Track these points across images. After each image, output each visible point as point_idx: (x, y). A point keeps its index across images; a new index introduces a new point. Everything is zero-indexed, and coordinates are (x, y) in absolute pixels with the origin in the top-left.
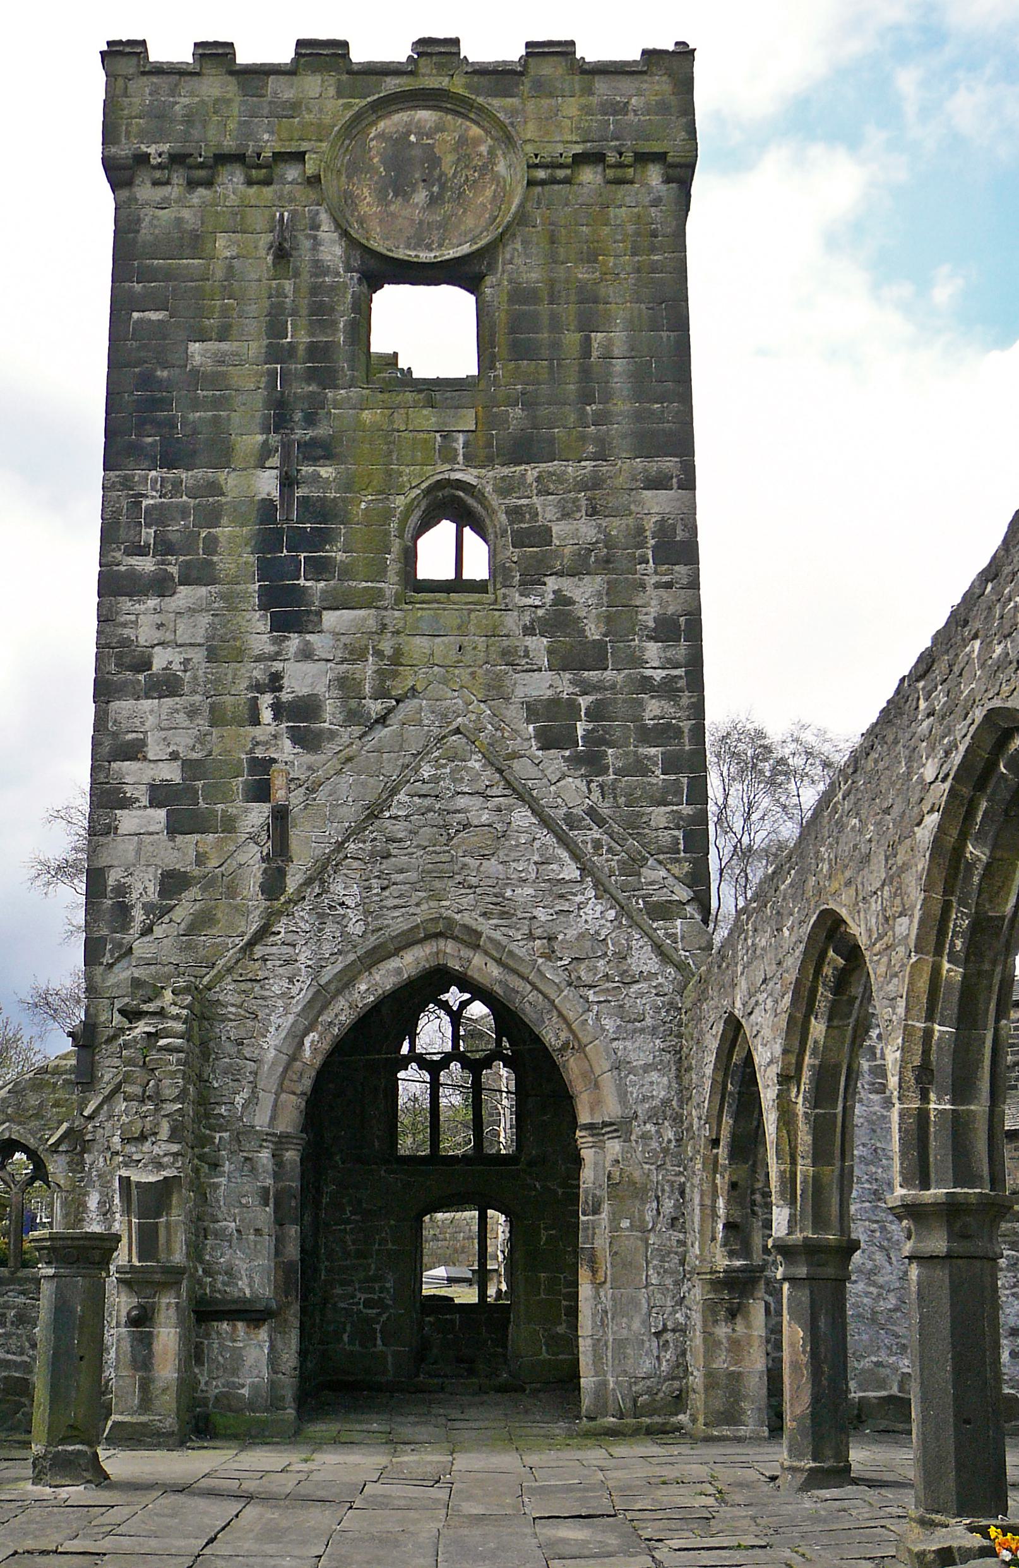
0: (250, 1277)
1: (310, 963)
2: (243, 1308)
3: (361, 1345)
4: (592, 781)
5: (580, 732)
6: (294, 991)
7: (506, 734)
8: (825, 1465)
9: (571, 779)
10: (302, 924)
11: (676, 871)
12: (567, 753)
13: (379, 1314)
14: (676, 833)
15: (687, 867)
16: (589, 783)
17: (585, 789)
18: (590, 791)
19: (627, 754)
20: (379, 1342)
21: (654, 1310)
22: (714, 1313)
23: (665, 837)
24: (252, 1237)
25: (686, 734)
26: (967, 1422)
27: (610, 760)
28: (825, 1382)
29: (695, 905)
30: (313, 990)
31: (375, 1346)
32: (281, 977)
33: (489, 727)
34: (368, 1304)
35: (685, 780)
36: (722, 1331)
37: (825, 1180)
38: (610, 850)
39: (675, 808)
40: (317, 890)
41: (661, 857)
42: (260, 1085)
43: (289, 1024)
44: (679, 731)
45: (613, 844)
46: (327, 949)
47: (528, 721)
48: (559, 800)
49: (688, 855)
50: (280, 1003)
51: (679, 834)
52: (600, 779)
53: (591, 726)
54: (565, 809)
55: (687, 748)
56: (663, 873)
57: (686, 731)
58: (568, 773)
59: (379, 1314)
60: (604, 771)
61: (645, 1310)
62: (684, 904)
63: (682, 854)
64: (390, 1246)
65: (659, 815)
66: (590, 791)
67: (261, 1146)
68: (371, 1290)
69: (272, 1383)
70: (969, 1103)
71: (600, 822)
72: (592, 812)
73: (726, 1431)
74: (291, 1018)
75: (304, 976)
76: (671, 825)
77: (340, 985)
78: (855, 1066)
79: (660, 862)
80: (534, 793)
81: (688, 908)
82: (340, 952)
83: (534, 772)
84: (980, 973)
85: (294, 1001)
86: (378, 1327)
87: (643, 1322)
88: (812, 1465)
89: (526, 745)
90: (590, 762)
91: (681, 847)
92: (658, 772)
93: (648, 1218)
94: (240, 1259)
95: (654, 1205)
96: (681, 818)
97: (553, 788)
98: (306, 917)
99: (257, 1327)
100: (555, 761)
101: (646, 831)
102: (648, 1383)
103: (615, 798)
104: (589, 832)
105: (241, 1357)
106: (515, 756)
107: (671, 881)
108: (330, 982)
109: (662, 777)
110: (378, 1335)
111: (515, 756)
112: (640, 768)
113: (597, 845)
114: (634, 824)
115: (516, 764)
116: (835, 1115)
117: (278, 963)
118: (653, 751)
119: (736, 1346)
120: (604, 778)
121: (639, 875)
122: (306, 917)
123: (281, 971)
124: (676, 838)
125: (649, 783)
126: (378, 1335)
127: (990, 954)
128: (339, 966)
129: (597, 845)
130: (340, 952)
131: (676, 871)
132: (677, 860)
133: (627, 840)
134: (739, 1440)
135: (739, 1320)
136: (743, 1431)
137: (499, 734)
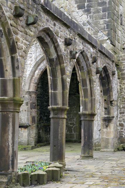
0: (24, 119)
1: (34, 57)
2: (23, 125)
3: (70, 133)
4: (88, 15)
5: (86, 5)
6: (32, 63)
7: (71, 7)
8: (85, 155)
9: (84, 15)
10: (33, 50)
11: (105, 33)
12: (83, 10)
13: (73, 126)
14: (105, 25)
15: (107, 32)
16: (87, 16)
17: (87, 17)
18: (88, 17)
19: (95, 9)
20: (73, 132)
21: (99, 126)
22: (103, 126)
23: (102, 26)
24: (24, 112)
25: (107, 3)
26: (55, 146)
27: (92, 10)
28: (86, 140)
29: (109, 40)
30: (35, 63)
31: (72, 132)
32: (29, 60)
33: (68, 6)
34: (71, 124)
35: (107, 13)
36: (105, 130)
37: (87, 101)
38: (91, 30)
39: (105, 19)
40: (36, 43)
41: (102, 30)
42: (26, 82)
43: (31, 70)
44: (106, 3)
45: (92, 29)
46: (38, 54)
47: (76, 4)
48: (82, 20)
49: (107, 29)
50: (29, 66)
51: (105, 25)
52: (90, 15)
53: (88, 3)
54: (83, 22)
55: (107, 6)
56: (102, 34)
57: (107, 2)
58: (83, 14)
59: (73, 126)
60: (90, 13)
61: (97, 126)
62: (107, 40)
63: (106, 29)
64: (75, 112)
65: (102, 21)
66: (88, 17)
67: (26, 94)
68: (72, 121)
69: (28, 140)
70: (56, 91)
71: (90, 24)
72: (88, 22)
73: (105, 150)
74: (31, 68)
75: (34, 60)
76: (104, 23)
77: (41, 61)
78: (92, 79)
79: (102, 31)
80: (77, 19)
81: (107, 41)
82: (40, 55)
83: (77, 14)
84: (53, 68)
85: (32, 65)
86: (73, 129)
87: (97, 128)
88: (84, 155)
89: (75, 9)
90: (88, 11)
91: (106, 28)
92: (101, 12)
93: (98, 107)
94: (22, 116)
95: (99, 104)
96: (106, 22)
97: (81, 17)
98: (34, 48)
99: (26, 129)
100: (81, 12)
101: (99, 25)
102: (98, 140)
103: (93, 18)
104: (87, 26)
105: (23, 135)
106: (73, 11)
107: (104, 35)
108: (39, 61)
109: (102, 13)
110: (73, 130)
111: (73, 11)
112: (98, 11)
113: (89, 29)
114: (96, 24)
115: (73, 13)
116: (87, 89)
117: (29, 58)
118: (100, 7)
119: (108, 133)
120: (91, 14)
121: (97, 35)
122: (34, 48)
123: (29, 59)
124: (105, 26)
125: (100, 15)
126: (73, 130)
127: (54, 65)
128: (40, 58)
129: (89, 29)
130: (40, 55)
131: (105, 33)
132: (105, 31)
133: (95, 27)
134: (107, 152)
135: (108, 127)
136: (108, 150)
137: (70, 7)
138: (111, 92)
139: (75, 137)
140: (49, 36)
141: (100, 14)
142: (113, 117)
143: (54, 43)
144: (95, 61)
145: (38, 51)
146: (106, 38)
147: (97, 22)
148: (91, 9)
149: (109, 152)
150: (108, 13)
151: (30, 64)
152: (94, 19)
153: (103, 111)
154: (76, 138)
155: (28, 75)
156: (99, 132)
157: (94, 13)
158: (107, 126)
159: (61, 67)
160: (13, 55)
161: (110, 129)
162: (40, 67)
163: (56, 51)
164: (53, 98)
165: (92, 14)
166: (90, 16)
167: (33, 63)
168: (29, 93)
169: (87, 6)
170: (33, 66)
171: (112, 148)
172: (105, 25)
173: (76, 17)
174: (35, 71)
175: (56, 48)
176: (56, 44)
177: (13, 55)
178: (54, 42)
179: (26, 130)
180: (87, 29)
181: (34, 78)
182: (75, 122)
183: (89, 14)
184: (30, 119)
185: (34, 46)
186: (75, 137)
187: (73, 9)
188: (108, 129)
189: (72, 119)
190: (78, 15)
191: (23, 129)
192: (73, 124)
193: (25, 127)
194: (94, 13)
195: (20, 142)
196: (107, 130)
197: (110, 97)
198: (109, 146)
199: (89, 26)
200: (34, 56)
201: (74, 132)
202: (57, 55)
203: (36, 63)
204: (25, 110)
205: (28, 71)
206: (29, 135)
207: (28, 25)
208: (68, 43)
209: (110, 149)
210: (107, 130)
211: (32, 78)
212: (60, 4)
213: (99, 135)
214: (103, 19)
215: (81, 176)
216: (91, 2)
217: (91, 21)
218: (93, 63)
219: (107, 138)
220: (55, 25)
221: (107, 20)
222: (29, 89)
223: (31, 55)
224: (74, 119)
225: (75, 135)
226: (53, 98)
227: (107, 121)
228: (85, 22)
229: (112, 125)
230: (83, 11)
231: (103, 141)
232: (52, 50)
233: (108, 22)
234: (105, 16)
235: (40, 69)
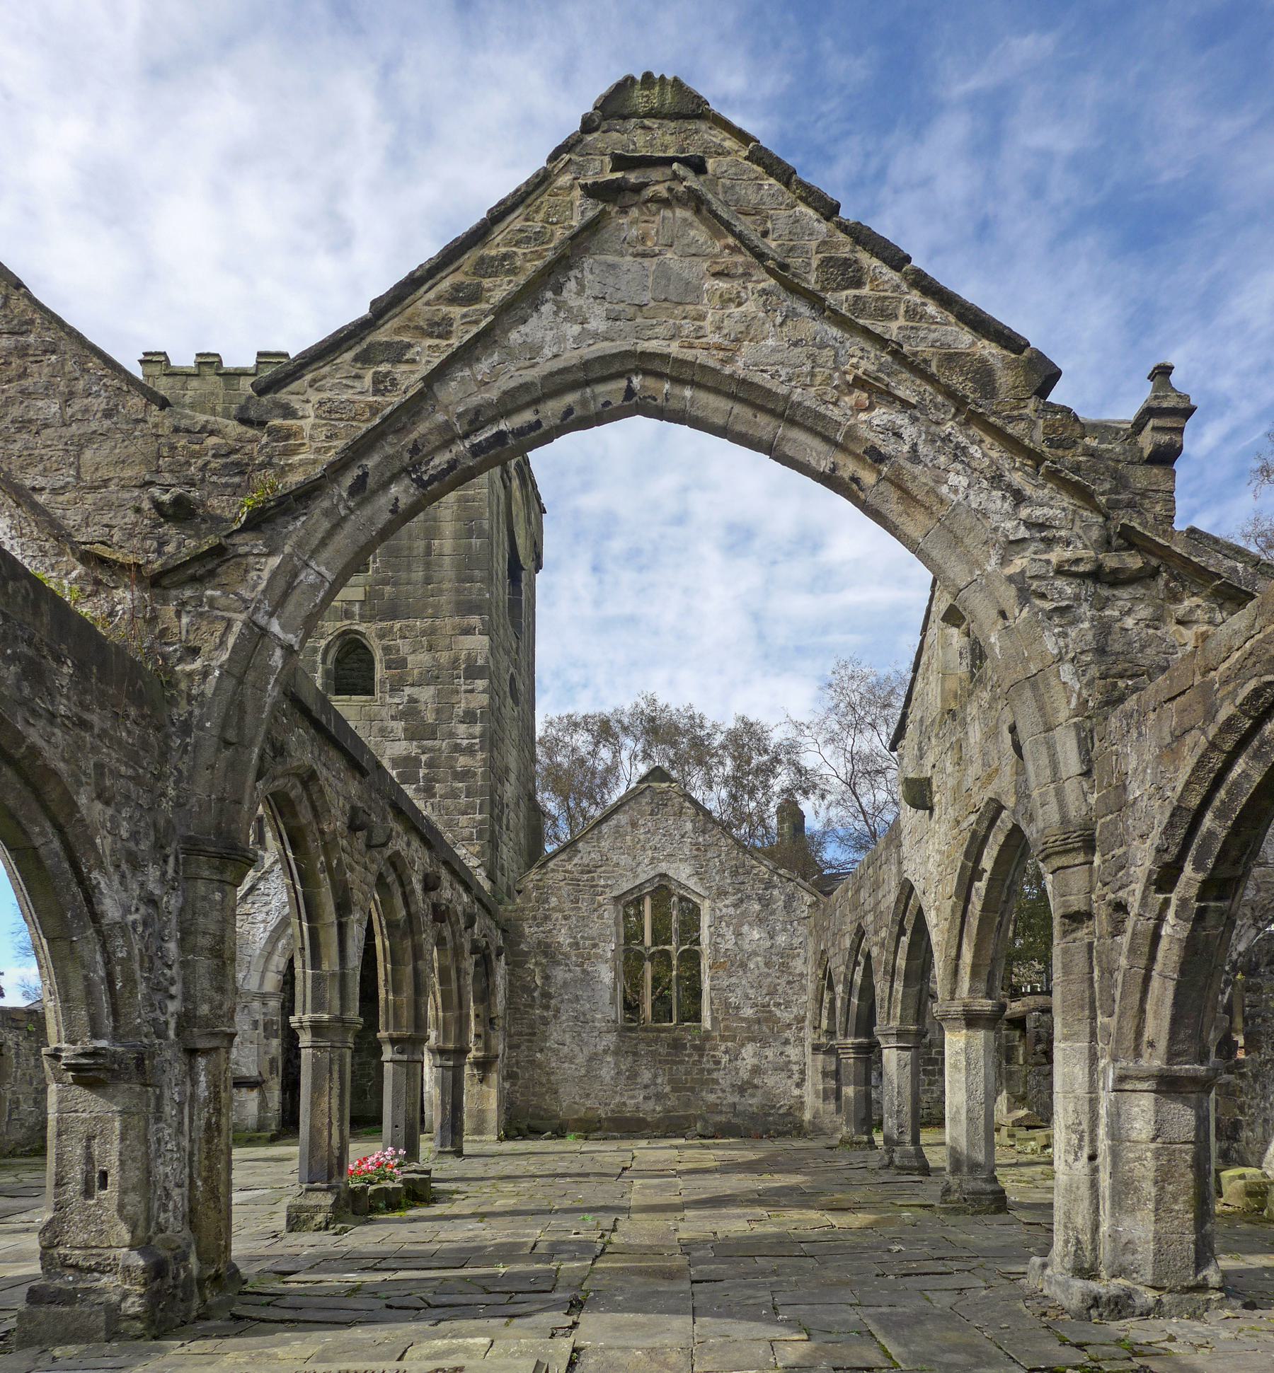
11: (471, 849)
23: (466, 832)
60: (434, 796)
65: (463, 820)
112: (454, 794)
118: (461, 785)
138: (992, 1046)
140: (395, 870)
142: (497, 1056)
143: (402, 885)
144: (470, 923)
147: (452, 820)
151: (263, 921)
155: (258, 951)
159: (413, 941)
160: (344, 920)
163: (407, 904)
164: (391, 1012)
175: (407, 898)
176: (408, 888)
177: (344, 920)
178: (403, 882)
184: (266, 1065)
191: (244, 1090)
197: (489, 1008)
202: (409, 913)
206: (263, 1105)
207: (369, 846)
208: (431, 884)
218: (466, 928)
220: (408, 844)
221: (478, 817)
222: (261, 985)
226: (391, 1012)
232: (398, 901)
233: (482, 822)
234: (474, 808)
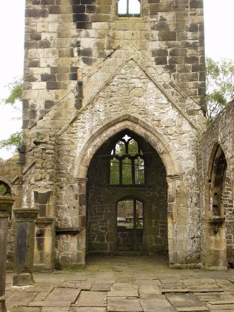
2: (69, 230)
5: (168, 59)
6: (85, 136)
10: (87, 116)
12: (164, 66)
13: (105, 232)
15: (199, 99)
16: (170, 75)
18: (170, 77)
22: (210, 232)
23: (193, 91)
27: (177, 68)
30: (90, 136)
34: (102, 229)
35: (199, 74)
36: (213, 238)
38: (176, 95)
40: (91, 107)
44: (197, 59)
46: (94, 124)
47: (153, 56)
50: (81, 140)
53: (171, 57)
56: (192, 101)
59: (105, 232)
60: (175, 71)
65: (191, 84)
66: (170, 77)
71: (173, 86)
72: (171, 83)
74: (84, 144)
75: (88, 132)
79: (191, 98)
81: (199, 111)
83: (154, 71)
89: (152, 63)
90: (171, 68)
92: (191, 71)
95: (190, 199)
97: (160, 76)
99: (74, 236)
100: (160, 68)
106: (148, 67)
107: (194, 104)
111: (148, 67)
112: (185, 70)
113: (173, 93)
114: (183, 87)
115: (149, 69)
118: (189, 65)
119: (217, 243)
120: (175, 73)
123: (80, 130)
131: (196, 101)
132: (196, 97)
135: (218, 234)
137: (144, 60)
139: (109, 248)
141: (189, 74)
145: (94, 120)
146: (198, 107)
147: (185, 84)
148: (175, 66)
149: (220, 271)
150: (201, 74)
151: (81, 138)
152: (180, 80)
153: (209, 210)
154: (110, 248)
156: (191, 241)
157: (180, 71)
158: (216, 233)
161: (220, 236)
162: (95, 143)
165: (177, 73)
166: (174, 76)
167: (87, 136)
168: (80, 181)
169: (169, 61)
170: (86, 141)
171: (224, 265)
172: (197, 90)
173: (153, 75)
174: (88, 148)
179: (75, 239)
180: (170, 93)
181: (85, 158)
182: (109, 227)
183: (173, 72)
185: (88, 111)
186: (109, 248)
187: (149, 63)
188: (217, 237)
189: (104, 221)
190: (156, 72)
191: (69, 236)
192: (106, 229)
193: (73, 233)
194: (180, 71)
195: (64, 257)
196: (216, 238)
198: (219, 262)
199: (172, 89)
200: (87, 126)
201: (107, 241)
203: (92, 137)
204: (74, 207)
205: (78, 147)
209: (222, 266)
210: (216, 238)
211: (83, 159)
212: (128, 55)
213: (192, 245)
214: (193, 81)
215: (50, 308)
216: (176, 55)
217: (175, 82)
219: (216, 251)
222: (79, 174)
223: (84, 124)
224: (107, 221)
225: (109, 246)
227: (217, 225)
228: (167, 83)
229: (223, 231)
230: (164, 68)
231: (211, 254)
235: (95, 146)
